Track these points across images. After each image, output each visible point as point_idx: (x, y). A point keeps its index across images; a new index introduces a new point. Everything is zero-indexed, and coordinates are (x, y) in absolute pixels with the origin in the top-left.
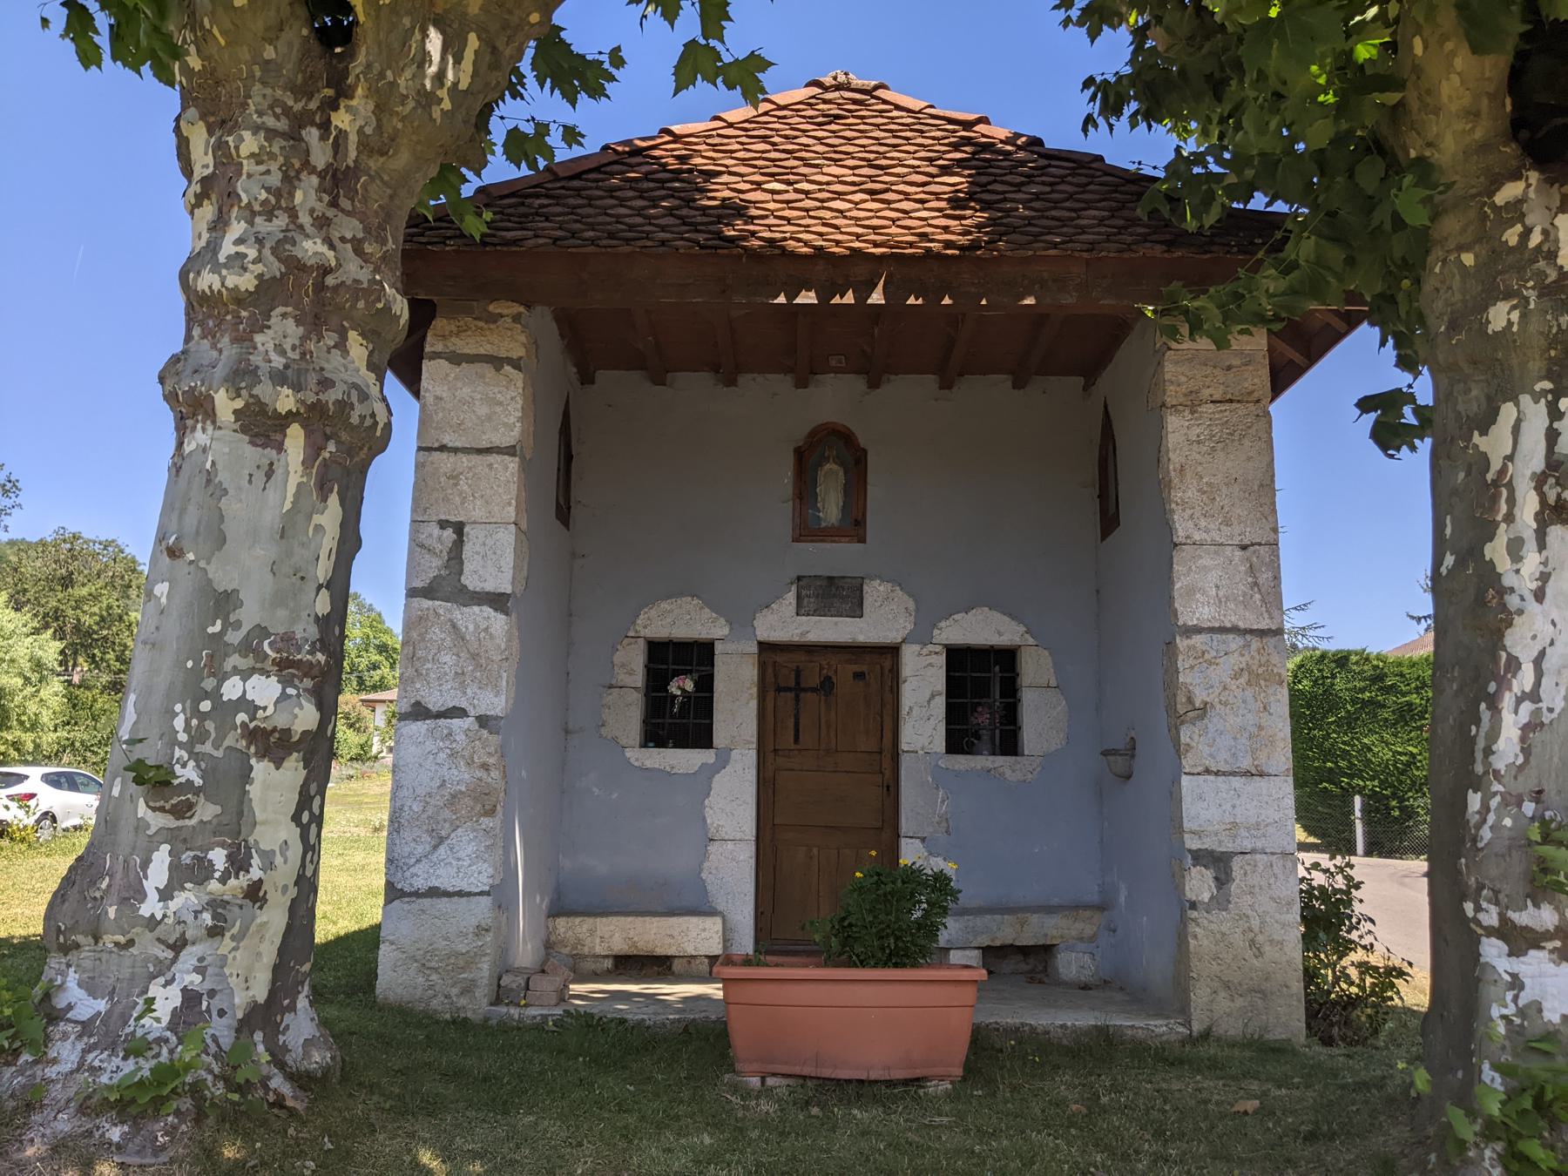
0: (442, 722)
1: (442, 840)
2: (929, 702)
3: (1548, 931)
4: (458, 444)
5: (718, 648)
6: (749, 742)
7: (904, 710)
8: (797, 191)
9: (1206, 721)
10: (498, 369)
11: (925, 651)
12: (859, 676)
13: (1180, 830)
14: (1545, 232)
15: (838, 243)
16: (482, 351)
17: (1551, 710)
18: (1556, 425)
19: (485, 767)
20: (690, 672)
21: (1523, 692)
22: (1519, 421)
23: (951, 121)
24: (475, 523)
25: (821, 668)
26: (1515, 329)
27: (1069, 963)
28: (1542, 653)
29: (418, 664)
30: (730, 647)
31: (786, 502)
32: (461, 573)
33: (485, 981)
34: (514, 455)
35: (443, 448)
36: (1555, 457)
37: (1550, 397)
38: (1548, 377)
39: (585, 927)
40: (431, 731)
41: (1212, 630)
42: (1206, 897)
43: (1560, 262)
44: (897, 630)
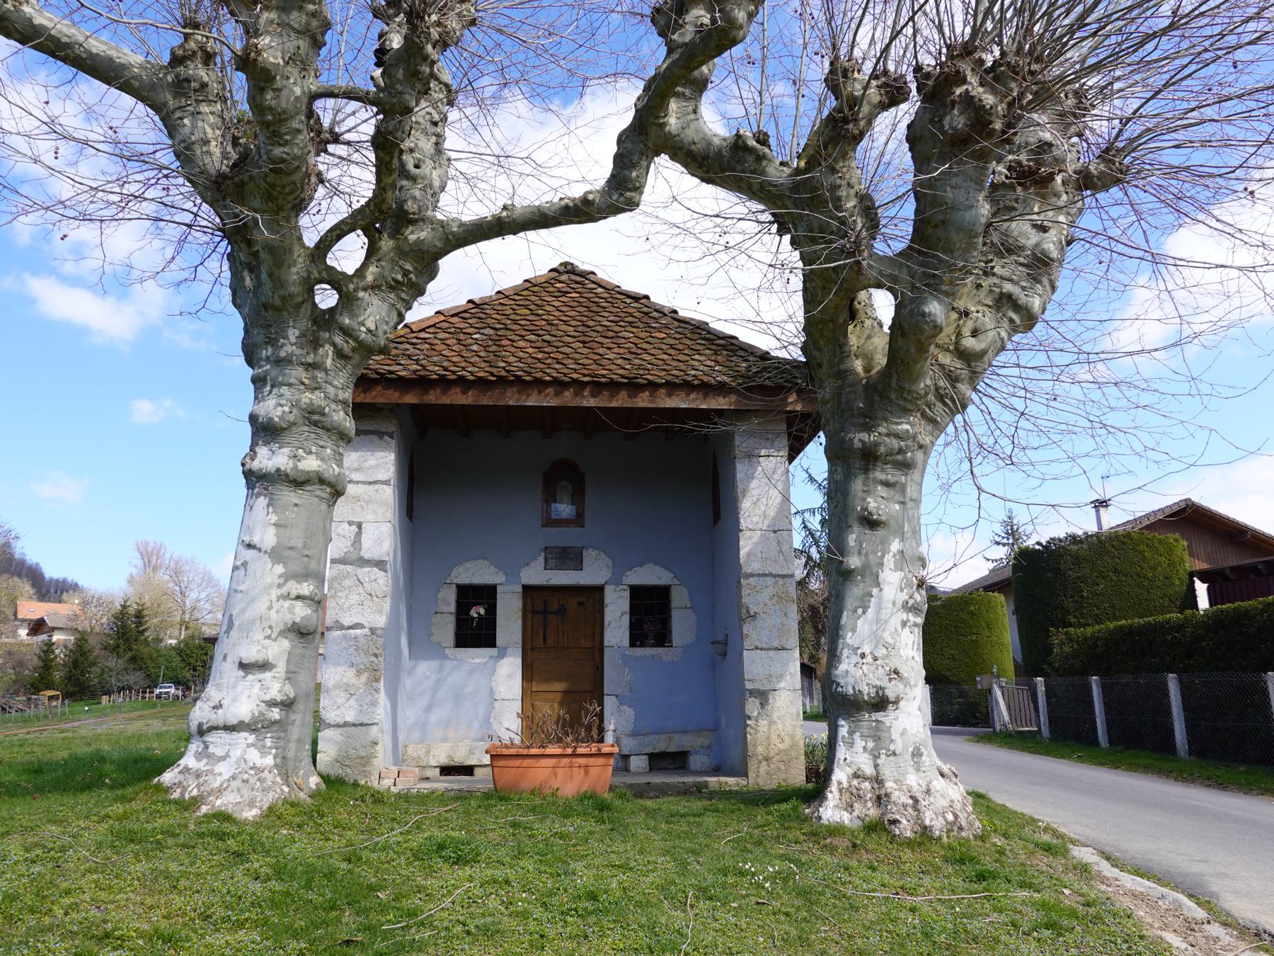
4: (359, 479)
5: (499, 589)
7: (606, 623)
8: (543, 340)
10: (381, 438)
13: (744, 680)
15: (565, 374)
30: (506, 588)
41: (759, 575)
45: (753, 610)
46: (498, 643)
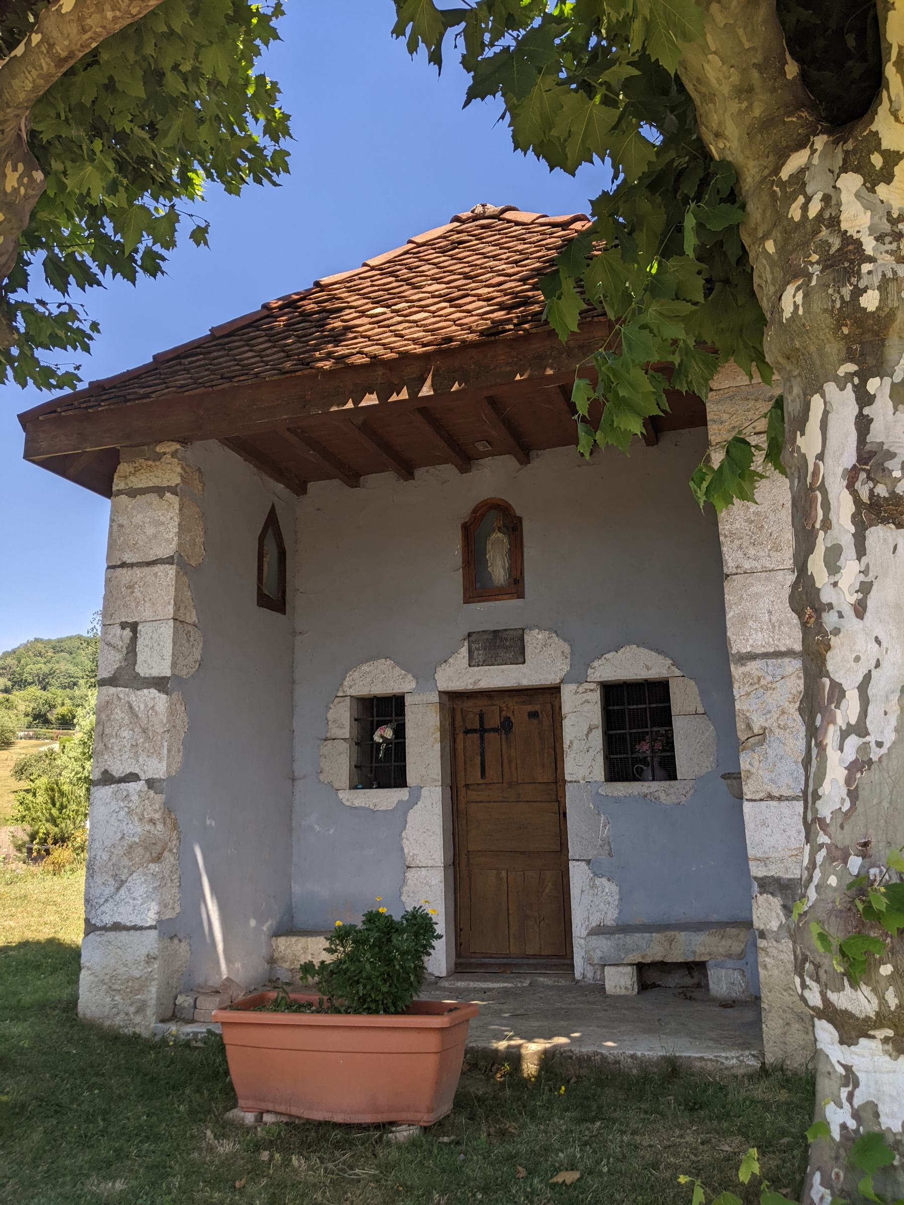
0: (123, 786)
1: (123, 882)
2: (587, 735)
3: (869, 1018)
4: (134, 560)
5: (408, 700)
6: (436, 780)
9: (765, 746)
10: (161, 497)
11: (581, 689)
12: (533, 715)
13: (745, 858)
14: (826, 199)
16: (151, 484)
17: (880, 744)
18: (866, 411)
19: (152, 821)
20: (390, 721)
21: (848, 724)
22: (826, 413)
23: (554, 225)
24: (145, 621)
25: (501, 710)
26: (801, 312)
27: (720, 980)
28: (868, 677)
29: (106, 739)
31: (458, 570)
32: (135, 663)
33: (153, 1002)
34: (172, 564)
35: (124, 565)
36: (868, 447)
37: (856, 380)
38: (851, 359)
39: (300, 946)
40: (115, 793)
41: (766, 655)
42: (774, 925)
43: (843, 227)
44: (555, 673)
45: (758, 722)
46: (409, 780)
